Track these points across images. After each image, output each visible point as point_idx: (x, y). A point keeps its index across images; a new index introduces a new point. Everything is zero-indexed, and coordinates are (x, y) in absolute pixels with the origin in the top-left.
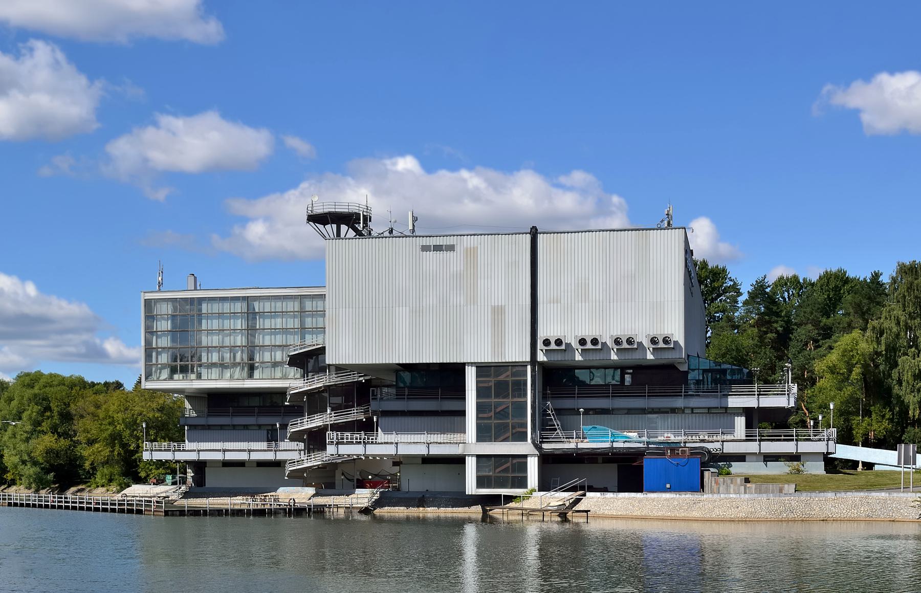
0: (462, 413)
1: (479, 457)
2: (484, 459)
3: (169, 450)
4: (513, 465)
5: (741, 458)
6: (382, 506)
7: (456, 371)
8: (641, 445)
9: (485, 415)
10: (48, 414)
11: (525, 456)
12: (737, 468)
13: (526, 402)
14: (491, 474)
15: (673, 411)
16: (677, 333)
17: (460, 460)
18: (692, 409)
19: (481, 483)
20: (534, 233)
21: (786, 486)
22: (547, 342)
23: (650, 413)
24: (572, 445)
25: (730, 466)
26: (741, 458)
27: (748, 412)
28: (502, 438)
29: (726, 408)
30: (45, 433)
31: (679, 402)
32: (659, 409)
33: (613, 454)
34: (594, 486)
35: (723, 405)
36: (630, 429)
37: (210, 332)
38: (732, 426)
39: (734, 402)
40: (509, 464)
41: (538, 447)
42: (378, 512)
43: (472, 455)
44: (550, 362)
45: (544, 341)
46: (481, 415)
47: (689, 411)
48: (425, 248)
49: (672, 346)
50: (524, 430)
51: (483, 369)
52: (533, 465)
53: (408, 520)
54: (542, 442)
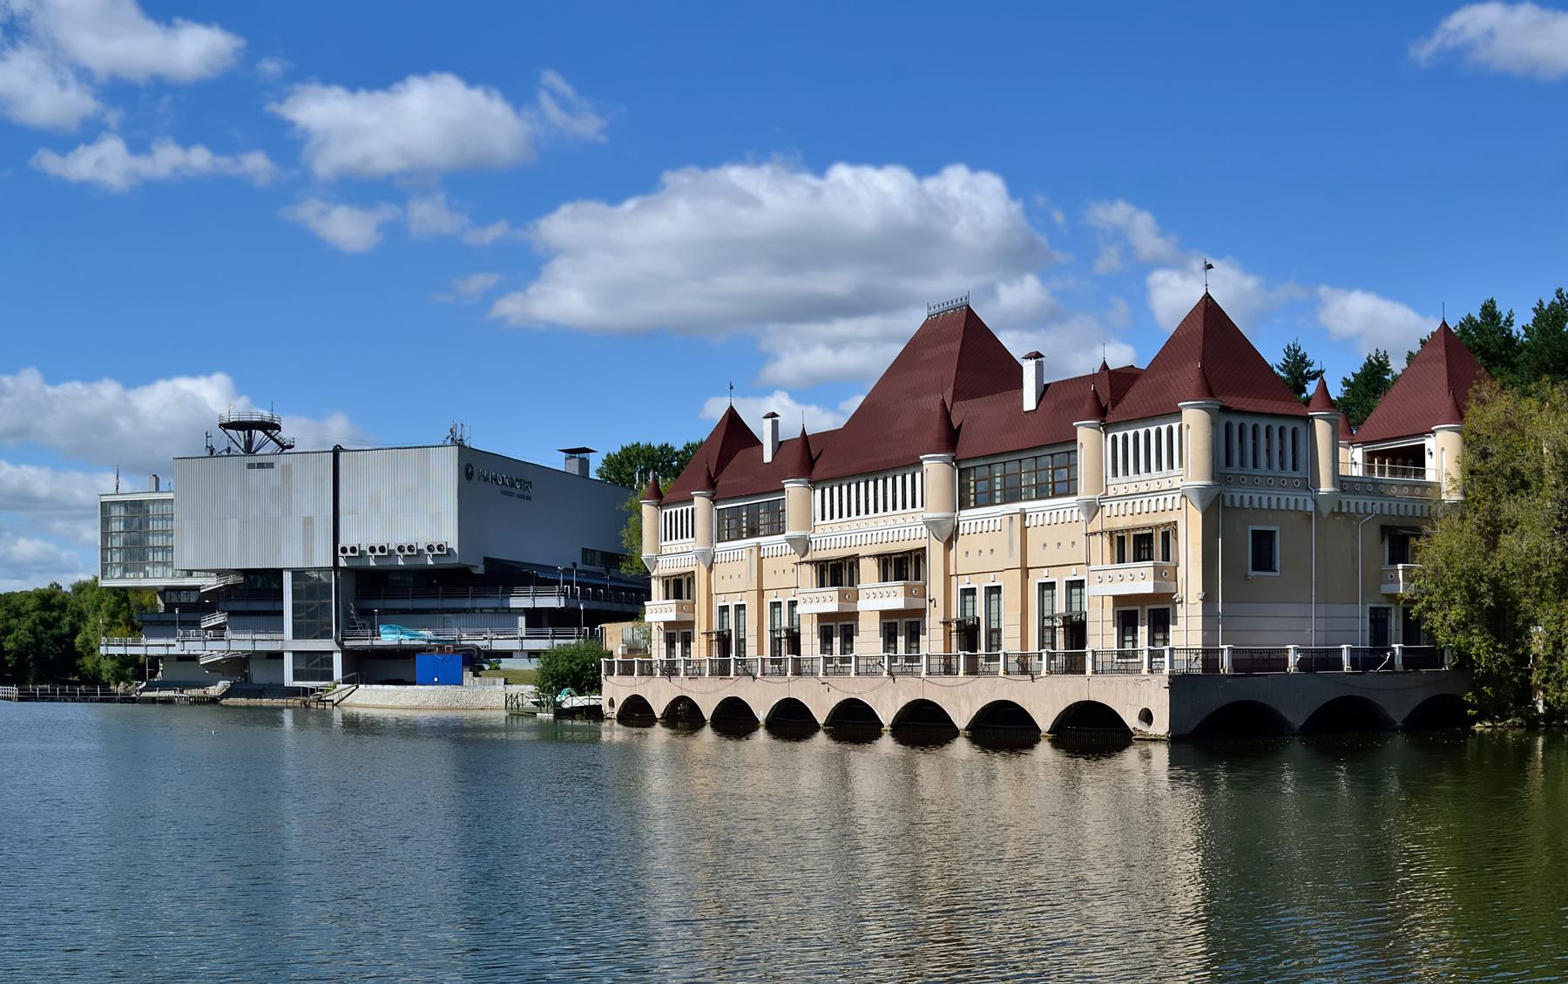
0: (281, 613)
1: (294, 652)
2: (299, 655)
3: (121, 645)
4: (322, 660)
5: (508, 654)
6: (227, 698)
7: (277, 574)
8: (424, 643)
9: (300, 615)
10: (125, 605)
11: (331, 652)
12: (505, 664)
13: (332, 603)
14: (304, 668)
15: (465, 611)
16: (453, 544)
17: (278, 656)
18: (481, 609)
19: (297, 676)
20: (337, 451)
21: (498, 680)
22: (344, 550)
23: (447, 613)
24: (368, 643)
25: (500, 662)
26: (508, 654)
27: (528, 612)
28: (312, 636)
29: (510, 608)
30: (120, 625)
31: (468, 603)
32: (454, 609)
33: (401, 650)
34: (406, 679)
35: (505, 606)
36: (423, 627)
37: (154, 533)
38: (516, 625)
39: (516, 603)
40: (318, 660)
41: (340, 644)
42: (223, 701)
43: (289, 651)
44: (380, 568)
45: (380, 548)
46: (297, 615)
47: (479, 611)
48: (251, 466)
49: (445, 553)
50: (330, 628)
51: (298, 574)
52: (337, 659)
53: (248, 707)
54: (343, 640)
